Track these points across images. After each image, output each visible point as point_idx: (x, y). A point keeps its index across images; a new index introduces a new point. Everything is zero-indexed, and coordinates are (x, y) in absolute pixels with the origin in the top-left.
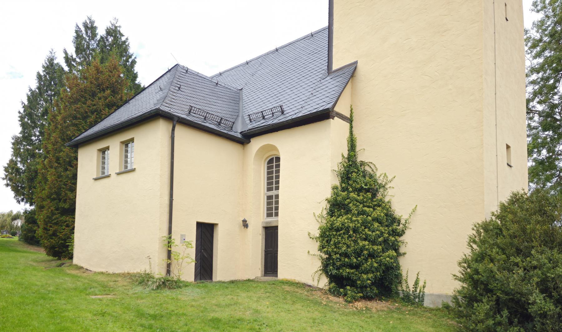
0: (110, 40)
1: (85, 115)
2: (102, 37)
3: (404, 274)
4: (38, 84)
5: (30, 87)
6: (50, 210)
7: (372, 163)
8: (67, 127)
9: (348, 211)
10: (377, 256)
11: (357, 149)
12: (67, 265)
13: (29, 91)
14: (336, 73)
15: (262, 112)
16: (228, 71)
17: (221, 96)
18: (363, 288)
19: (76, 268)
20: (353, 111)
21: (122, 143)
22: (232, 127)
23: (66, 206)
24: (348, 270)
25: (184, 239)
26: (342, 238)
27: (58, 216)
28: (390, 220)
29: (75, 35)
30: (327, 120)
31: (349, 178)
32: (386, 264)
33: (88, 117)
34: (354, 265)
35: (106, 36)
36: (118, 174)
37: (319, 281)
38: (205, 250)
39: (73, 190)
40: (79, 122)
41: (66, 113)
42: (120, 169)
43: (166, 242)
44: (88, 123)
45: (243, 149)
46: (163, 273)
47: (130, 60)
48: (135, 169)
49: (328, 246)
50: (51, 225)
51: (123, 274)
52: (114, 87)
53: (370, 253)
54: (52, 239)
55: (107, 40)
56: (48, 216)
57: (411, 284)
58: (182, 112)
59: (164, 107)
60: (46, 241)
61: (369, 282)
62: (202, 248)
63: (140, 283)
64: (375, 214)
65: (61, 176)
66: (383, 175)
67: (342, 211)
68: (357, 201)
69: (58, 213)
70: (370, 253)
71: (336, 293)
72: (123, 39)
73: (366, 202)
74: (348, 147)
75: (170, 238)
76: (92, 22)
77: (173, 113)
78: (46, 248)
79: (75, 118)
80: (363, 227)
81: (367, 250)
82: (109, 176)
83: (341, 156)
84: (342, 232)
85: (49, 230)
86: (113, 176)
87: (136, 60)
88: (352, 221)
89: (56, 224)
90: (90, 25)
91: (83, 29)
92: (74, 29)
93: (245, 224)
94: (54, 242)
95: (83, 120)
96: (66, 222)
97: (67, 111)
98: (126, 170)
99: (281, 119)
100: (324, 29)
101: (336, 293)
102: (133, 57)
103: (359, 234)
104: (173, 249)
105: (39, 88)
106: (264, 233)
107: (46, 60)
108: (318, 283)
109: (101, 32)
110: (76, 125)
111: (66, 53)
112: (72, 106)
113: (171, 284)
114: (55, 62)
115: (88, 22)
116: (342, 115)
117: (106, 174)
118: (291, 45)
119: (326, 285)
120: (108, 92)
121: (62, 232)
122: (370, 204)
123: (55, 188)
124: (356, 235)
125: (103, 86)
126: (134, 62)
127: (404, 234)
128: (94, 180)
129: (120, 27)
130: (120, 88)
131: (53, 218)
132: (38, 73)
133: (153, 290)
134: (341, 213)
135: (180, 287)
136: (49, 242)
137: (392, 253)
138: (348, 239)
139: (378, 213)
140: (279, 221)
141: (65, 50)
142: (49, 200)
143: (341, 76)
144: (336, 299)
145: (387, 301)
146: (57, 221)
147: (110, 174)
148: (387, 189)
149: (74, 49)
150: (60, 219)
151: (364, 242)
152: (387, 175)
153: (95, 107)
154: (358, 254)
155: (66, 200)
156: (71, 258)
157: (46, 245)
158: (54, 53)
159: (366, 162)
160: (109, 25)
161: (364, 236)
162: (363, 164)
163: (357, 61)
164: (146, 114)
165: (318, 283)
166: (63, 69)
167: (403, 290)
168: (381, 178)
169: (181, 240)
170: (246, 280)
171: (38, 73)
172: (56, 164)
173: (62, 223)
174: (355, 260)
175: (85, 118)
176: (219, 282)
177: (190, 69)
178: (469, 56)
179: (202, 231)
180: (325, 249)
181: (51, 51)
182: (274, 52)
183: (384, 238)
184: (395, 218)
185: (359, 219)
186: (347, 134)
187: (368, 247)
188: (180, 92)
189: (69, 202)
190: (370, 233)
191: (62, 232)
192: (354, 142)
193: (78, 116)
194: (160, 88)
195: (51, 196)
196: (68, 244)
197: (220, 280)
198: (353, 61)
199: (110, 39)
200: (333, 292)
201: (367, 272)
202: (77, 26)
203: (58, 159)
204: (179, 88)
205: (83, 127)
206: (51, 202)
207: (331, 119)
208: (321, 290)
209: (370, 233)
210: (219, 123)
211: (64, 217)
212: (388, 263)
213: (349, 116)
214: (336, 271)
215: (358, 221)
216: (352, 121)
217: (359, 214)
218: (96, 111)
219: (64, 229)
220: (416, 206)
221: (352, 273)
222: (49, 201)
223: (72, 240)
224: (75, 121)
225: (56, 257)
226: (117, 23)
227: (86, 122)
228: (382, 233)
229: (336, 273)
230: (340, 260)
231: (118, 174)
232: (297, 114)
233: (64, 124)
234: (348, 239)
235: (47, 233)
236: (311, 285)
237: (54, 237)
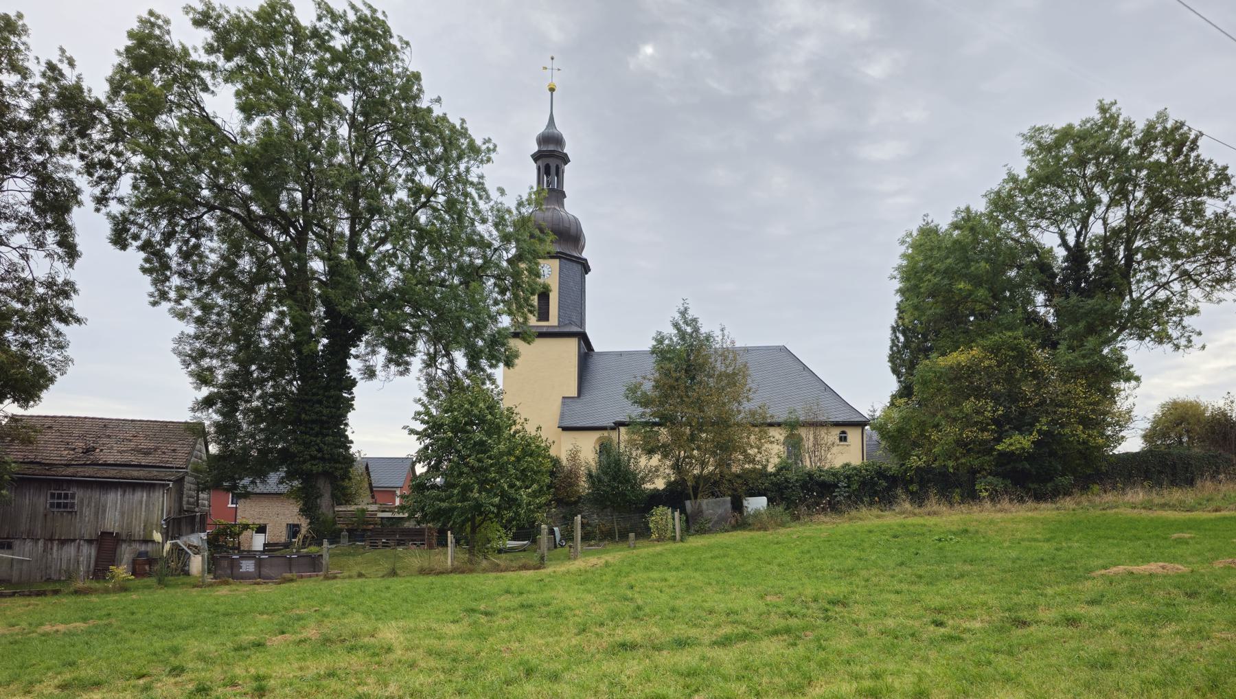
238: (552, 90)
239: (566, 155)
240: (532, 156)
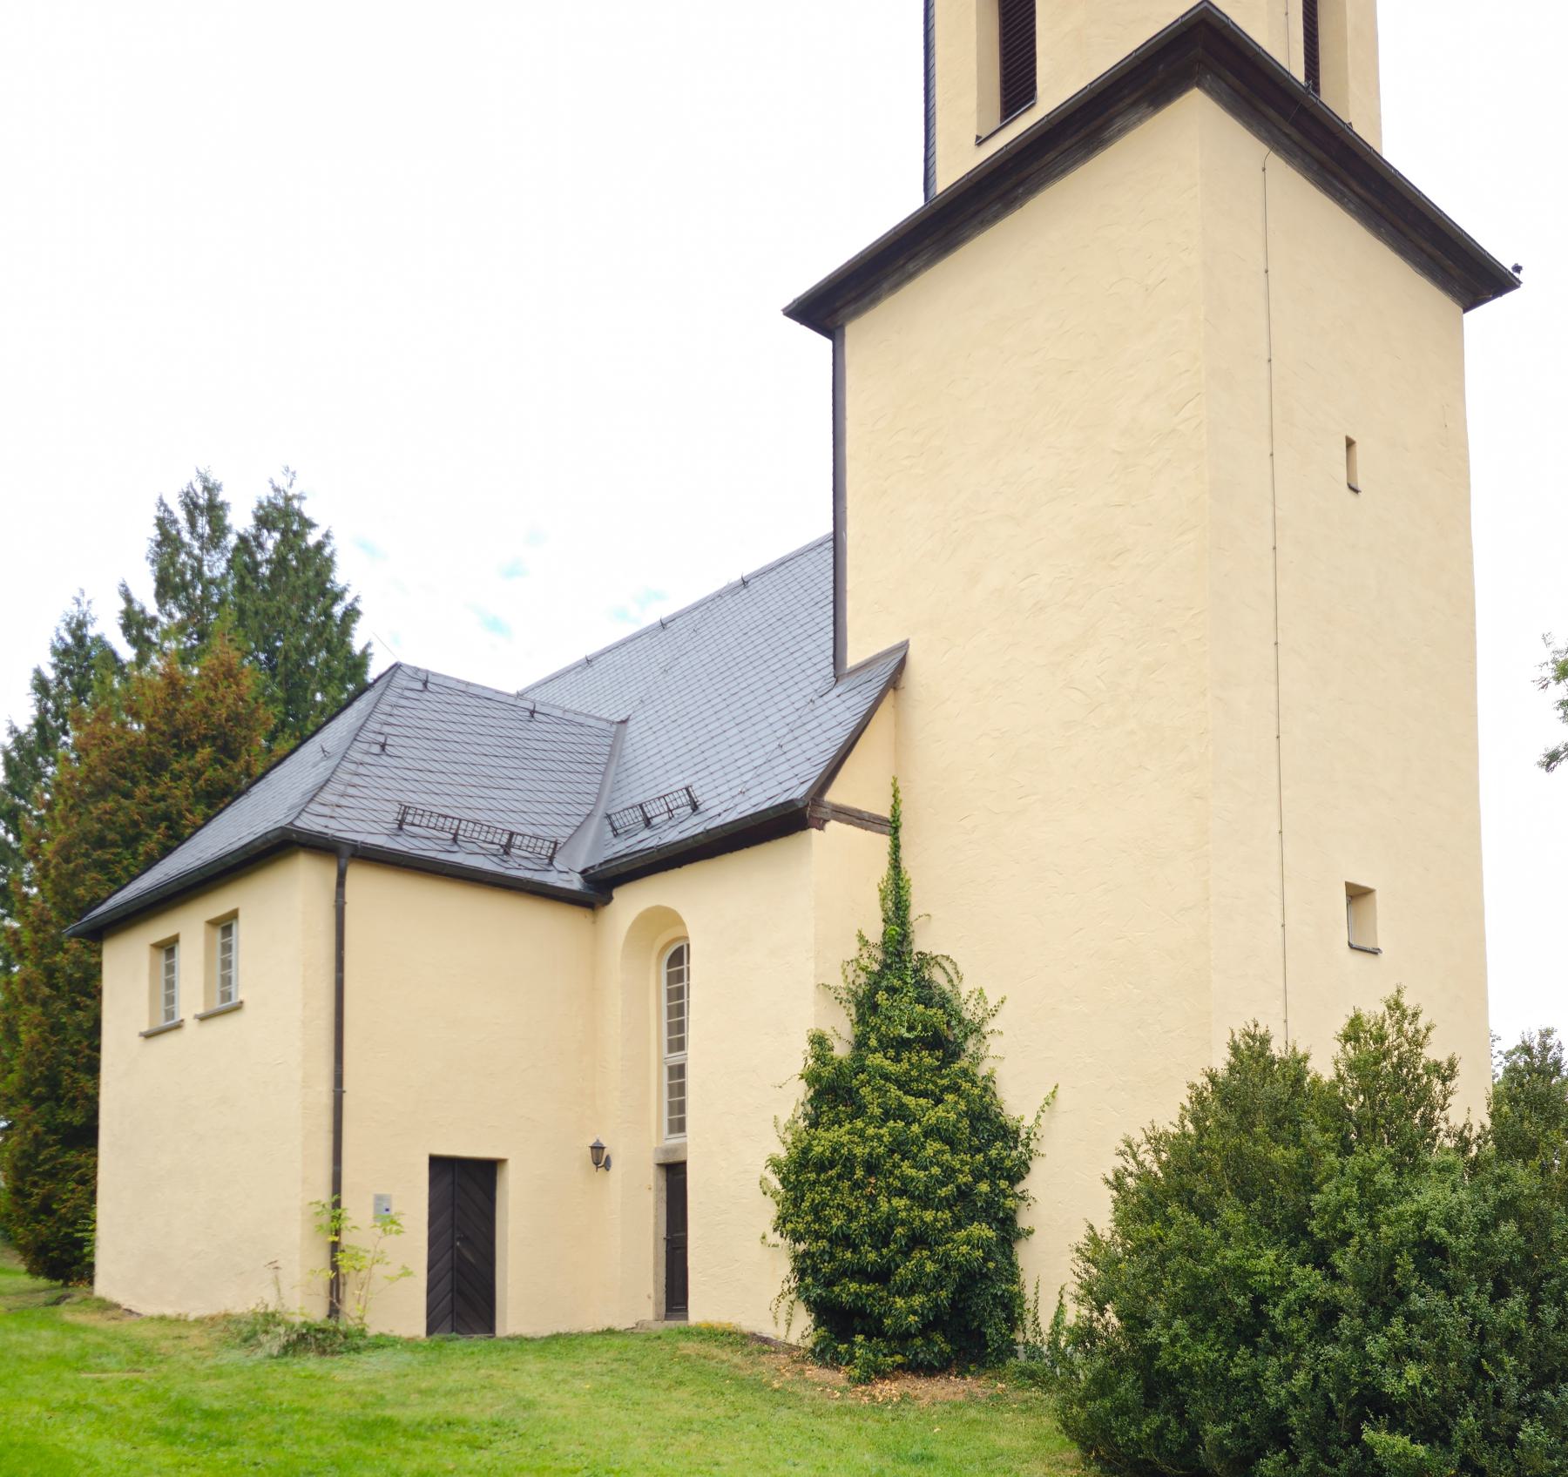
0: (270, 545)
1: (131, 832)
2: (243, 539)
3: (1029, 1293)
4: (34, 712)
5: (11, 722)
6: (30, 1134)
7: (948, 958)
8: (74, 874)
9: (860, 1110)
10: (937, 1243)
11: (914, 913)
12: (76, 1299)
13: (7, 732)
14: (853, 677)
16: (609, 650)
17: (539, 755)
18: (903, 1337)
19: (99, 1307)
20: (900, 796)
21: (213, 923)
22: (551, 859)
23: (77, 1119)
24: (853, 1286)
25: (387, 1210)
26: (835, 1190)
27: (52, 1151)
28: (988, 1130)
29: (155, 533)
30: (804, 832)
31: (875, 1007)
32: (960, 1267)
33: (136, 839)
35: (254, 531)
36: (203, 1018)
37: (789, 1325)
38: (464, 1239)
39: (93, 1068)
40: (113, 854)
41: (69, 832)
42: (152, 1018)
43: (325, 1219)
44: (142, 858)
45: (594, 922)
46: (317, 1313)
48: (241, 1003)
49: (798, 1216)
50: (36, 1178)
51: (212, 1319)
52: (225, 734)
53: (914, 1234)
54: (39, 1222)
55: (261, 546)
56: (24, 1152)
57: (1046, 1324)
58: (377, 828)
59: (313, 818)
60: (20, 1230)
61: (912, 1318)
62: (457, 1236)
63: (246, 1340)
64: (935, 1115)
65: (63, 1027)
66: (975, 996)
67: (841, 1108)
68: (886, 1077)
69: (56, 1142)
70: (914, 1234)
71: (828, 1357)
72: (312, 538)
73: (917, 1081)
74: (885, 910)
75: (337, 1204)
76: (211, 490)
78: (24, 1250)
79: (101, 843)
80: (897, 1157)
81: (903, 1223)
82: (178, 1026)
83: (857, 938)
84: (832, 1173)
85: (30, 1195)
86: (191, 1024)
87: (359, 606)
88: (864, 1139)
89: (51, 1175)
90: (206, 496)
91: (180, 515)
92: (153, 513)
93: (600, 1157)
94: (45, 1231)
95: (127, 849)
96: (78, 1167)
97: (72, 824)
98: (226, 1007)
99: (692, 827)
100: (819, 545)
101: (828, 1357)
102: (349, 598)
103: (885, 1177)
104: (346, 1239)
105: (40, 724)
106: (663, 1184)
107: (63, 625)
108: (788, 1330)
109: (240, 520)
110: (103, 866)
111: (129, 599)
112: (91, 807)
113: (328, 1341)
114: (92, 632)
115: (199, 488)
116: (859, 811)
117: (234, 1001)
118: (783, 567)
119: (806, 1333)
120: (206, 752)
121: (67, 1200)
122: (930, 1086)
123: (42, 1065)
124: (877, 1179)
125: (189, 737)
126: (352, 614)
127: (1027, 1173)
128: (142, 1038)
129: (301, 498)
130: (245, 738)
131: (41, 1157)
132: (38, 672)
133: (271, 1356)
134: (837, 1114)
135: (357, 1350)
136: (32, 1231)
137: (983, 1231)
138: (852, 1194)
139: (947, 1112)
140: (689, 1143)
141: (123, 586)
142: (26, 1104)
143: (859, 689)
144: (827, 1375)
145: (978, 1377)
146: (53, 1168)
147: (182, 1021)
148: (985, 1038)
149: (152, 586)
150: (61, 1160)
151: (895, 1202)
152: (986, 993)
153: (162, 805)
154: (881, 1236)
155: (74, 1099)
156: (91, 1283)
157: (22, 1242)
158: (89, 602)
159: (934, 954)
160: (266, 493)
161: (897, 1184)
162: (926, 960)
164: (257, 843)
165: (788, 1330)
166: (114, 654)
167: (1027, 1343)
168: (971, 1006)
169: (376, 1211)
170: (602, 1333)
171: (38, 672)
172: (47, 991)
173: (68, 1171)
174: (872, 1256)
175: (131, 842)
176: (511, 1339)
177: (434, 675)
178: (1174, 631)
179: (453, 1183)
180: (789, 1226)
181: (78, 595)
182: (736, 591)
183: (958, 1187)
184: (1003, 1127)
185: (884, 1131)
186: (883, 869)
187: (904, 1214)
188: (385, 760)
189: (83, 1106)
190: (912, 1172)
191: (67, 1200)
192: (902, 893)
193: (111, 836)
194: (324, 751)
195: (31, 1090)
196: (79, 1235)
197: (518, 1333)
199: (271, 540)
200: (824, 1355)
201: (908, 1290)
202: (162, 503)
203: (50, 972)
204: (383, 746)
205: (126, 869)
206: (34, 1108)
207: (814, 831)
208: (791, 1349)
209: (912, 1172)
210: (507, 848)
211: (73, 1152)
212: (966, 1260)
213: (887, 814)
214: (819, 1291)
215: (880, 1138)
216: (896, 829)
217: (887, 1115)
218: (166, 817)
219: (73, 1191)
220: (1056, 1087)
221: (868, 1295)
222: (28, 1106)
223: (89, 1224)
224: (99, 852)
225: (57, 1279)
226: (291, 485)
227: (135, 855)
228: (950, 1173)
229: (819, 1295)
230: (832, 1258)
231: (203, 1018)
232: (724, 815)
233: (65, 866)
234: (852, 1194)
235: (25, 1205)
236: (771, 1336)
237: (43, 1217)
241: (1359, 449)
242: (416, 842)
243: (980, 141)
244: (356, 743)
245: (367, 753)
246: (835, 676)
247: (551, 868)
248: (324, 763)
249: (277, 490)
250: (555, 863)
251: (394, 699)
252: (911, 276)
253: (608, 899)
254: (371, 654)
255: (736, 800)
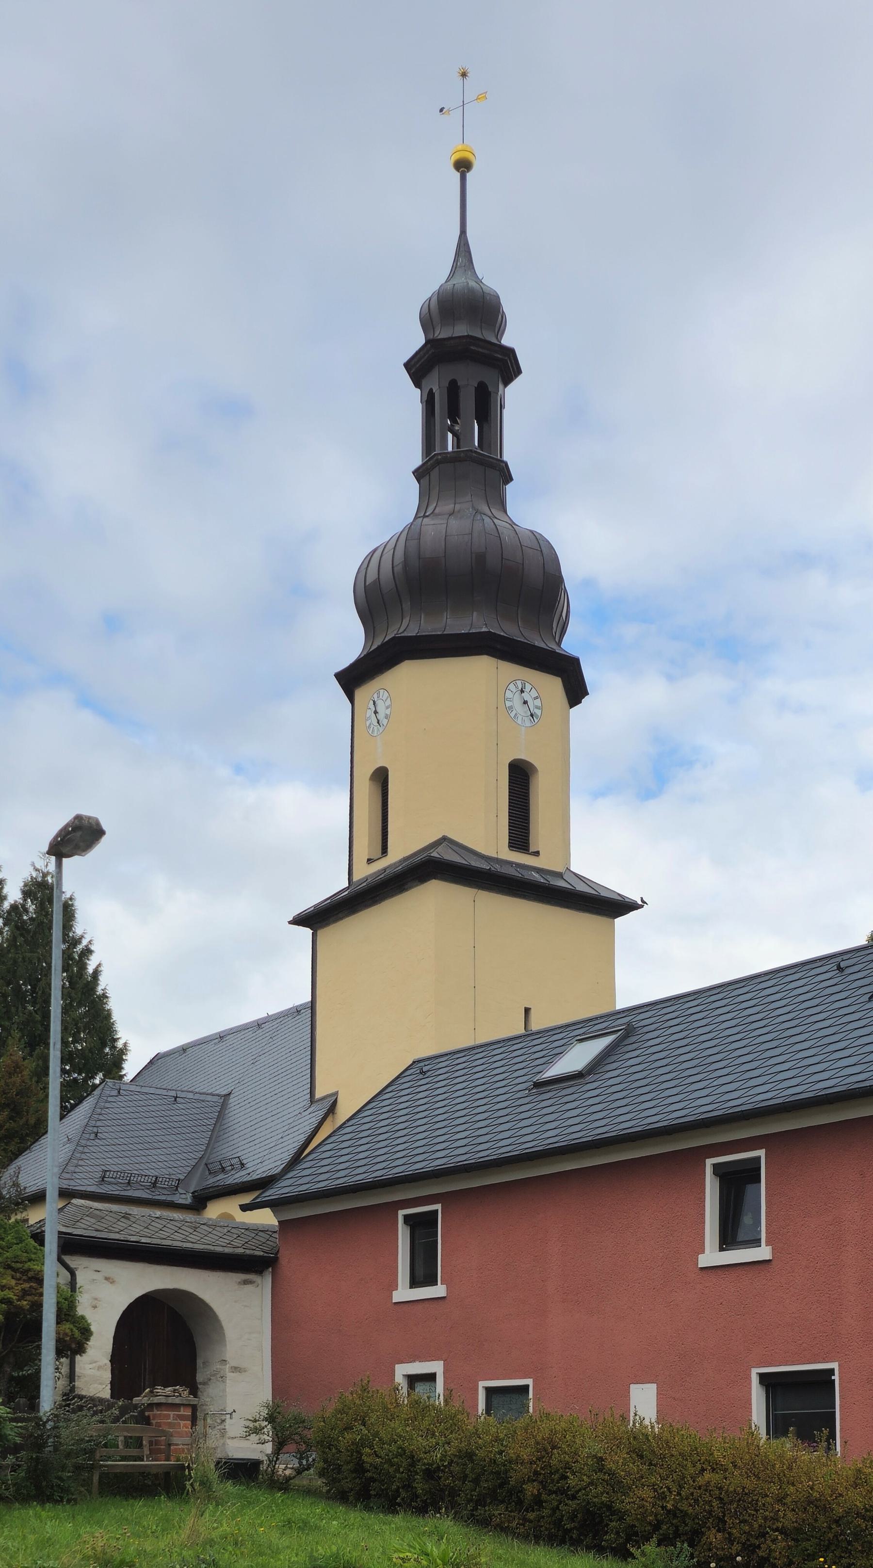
15: (220, 1161)
22: (177, 1187)
34: (757, 1551)
35: (22, 902)
47: (80, 947)
77: (75, 1188)
87: (92, 948)
102: (85, 942)
163: (338, 1092)
198: (333, 1091)
238: (463, 166)
239: (510, 353)
240: (408, 366)
241: (533, 1014)
242: (109, 1187)
243: (370, 861)
244: (83, 1135)
245: (89, 1139)
246: (310, 1101)
247: (177, 1192)
248: (68, 1145)
249: (37, 870)
250: (179, 1189)
251: (103, 1104)
252: (341, 919)
253: (205, 1207)
254: (101, 971)
255: (258, 1167)
